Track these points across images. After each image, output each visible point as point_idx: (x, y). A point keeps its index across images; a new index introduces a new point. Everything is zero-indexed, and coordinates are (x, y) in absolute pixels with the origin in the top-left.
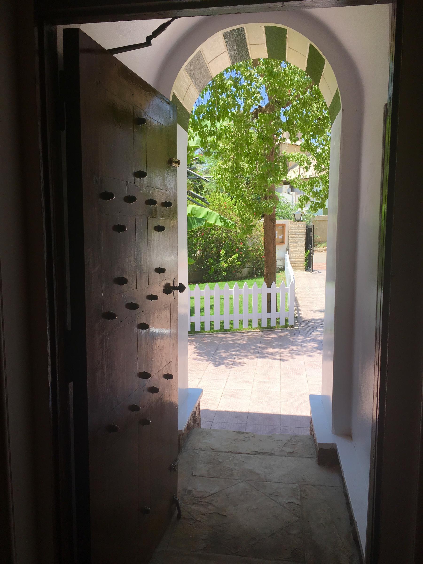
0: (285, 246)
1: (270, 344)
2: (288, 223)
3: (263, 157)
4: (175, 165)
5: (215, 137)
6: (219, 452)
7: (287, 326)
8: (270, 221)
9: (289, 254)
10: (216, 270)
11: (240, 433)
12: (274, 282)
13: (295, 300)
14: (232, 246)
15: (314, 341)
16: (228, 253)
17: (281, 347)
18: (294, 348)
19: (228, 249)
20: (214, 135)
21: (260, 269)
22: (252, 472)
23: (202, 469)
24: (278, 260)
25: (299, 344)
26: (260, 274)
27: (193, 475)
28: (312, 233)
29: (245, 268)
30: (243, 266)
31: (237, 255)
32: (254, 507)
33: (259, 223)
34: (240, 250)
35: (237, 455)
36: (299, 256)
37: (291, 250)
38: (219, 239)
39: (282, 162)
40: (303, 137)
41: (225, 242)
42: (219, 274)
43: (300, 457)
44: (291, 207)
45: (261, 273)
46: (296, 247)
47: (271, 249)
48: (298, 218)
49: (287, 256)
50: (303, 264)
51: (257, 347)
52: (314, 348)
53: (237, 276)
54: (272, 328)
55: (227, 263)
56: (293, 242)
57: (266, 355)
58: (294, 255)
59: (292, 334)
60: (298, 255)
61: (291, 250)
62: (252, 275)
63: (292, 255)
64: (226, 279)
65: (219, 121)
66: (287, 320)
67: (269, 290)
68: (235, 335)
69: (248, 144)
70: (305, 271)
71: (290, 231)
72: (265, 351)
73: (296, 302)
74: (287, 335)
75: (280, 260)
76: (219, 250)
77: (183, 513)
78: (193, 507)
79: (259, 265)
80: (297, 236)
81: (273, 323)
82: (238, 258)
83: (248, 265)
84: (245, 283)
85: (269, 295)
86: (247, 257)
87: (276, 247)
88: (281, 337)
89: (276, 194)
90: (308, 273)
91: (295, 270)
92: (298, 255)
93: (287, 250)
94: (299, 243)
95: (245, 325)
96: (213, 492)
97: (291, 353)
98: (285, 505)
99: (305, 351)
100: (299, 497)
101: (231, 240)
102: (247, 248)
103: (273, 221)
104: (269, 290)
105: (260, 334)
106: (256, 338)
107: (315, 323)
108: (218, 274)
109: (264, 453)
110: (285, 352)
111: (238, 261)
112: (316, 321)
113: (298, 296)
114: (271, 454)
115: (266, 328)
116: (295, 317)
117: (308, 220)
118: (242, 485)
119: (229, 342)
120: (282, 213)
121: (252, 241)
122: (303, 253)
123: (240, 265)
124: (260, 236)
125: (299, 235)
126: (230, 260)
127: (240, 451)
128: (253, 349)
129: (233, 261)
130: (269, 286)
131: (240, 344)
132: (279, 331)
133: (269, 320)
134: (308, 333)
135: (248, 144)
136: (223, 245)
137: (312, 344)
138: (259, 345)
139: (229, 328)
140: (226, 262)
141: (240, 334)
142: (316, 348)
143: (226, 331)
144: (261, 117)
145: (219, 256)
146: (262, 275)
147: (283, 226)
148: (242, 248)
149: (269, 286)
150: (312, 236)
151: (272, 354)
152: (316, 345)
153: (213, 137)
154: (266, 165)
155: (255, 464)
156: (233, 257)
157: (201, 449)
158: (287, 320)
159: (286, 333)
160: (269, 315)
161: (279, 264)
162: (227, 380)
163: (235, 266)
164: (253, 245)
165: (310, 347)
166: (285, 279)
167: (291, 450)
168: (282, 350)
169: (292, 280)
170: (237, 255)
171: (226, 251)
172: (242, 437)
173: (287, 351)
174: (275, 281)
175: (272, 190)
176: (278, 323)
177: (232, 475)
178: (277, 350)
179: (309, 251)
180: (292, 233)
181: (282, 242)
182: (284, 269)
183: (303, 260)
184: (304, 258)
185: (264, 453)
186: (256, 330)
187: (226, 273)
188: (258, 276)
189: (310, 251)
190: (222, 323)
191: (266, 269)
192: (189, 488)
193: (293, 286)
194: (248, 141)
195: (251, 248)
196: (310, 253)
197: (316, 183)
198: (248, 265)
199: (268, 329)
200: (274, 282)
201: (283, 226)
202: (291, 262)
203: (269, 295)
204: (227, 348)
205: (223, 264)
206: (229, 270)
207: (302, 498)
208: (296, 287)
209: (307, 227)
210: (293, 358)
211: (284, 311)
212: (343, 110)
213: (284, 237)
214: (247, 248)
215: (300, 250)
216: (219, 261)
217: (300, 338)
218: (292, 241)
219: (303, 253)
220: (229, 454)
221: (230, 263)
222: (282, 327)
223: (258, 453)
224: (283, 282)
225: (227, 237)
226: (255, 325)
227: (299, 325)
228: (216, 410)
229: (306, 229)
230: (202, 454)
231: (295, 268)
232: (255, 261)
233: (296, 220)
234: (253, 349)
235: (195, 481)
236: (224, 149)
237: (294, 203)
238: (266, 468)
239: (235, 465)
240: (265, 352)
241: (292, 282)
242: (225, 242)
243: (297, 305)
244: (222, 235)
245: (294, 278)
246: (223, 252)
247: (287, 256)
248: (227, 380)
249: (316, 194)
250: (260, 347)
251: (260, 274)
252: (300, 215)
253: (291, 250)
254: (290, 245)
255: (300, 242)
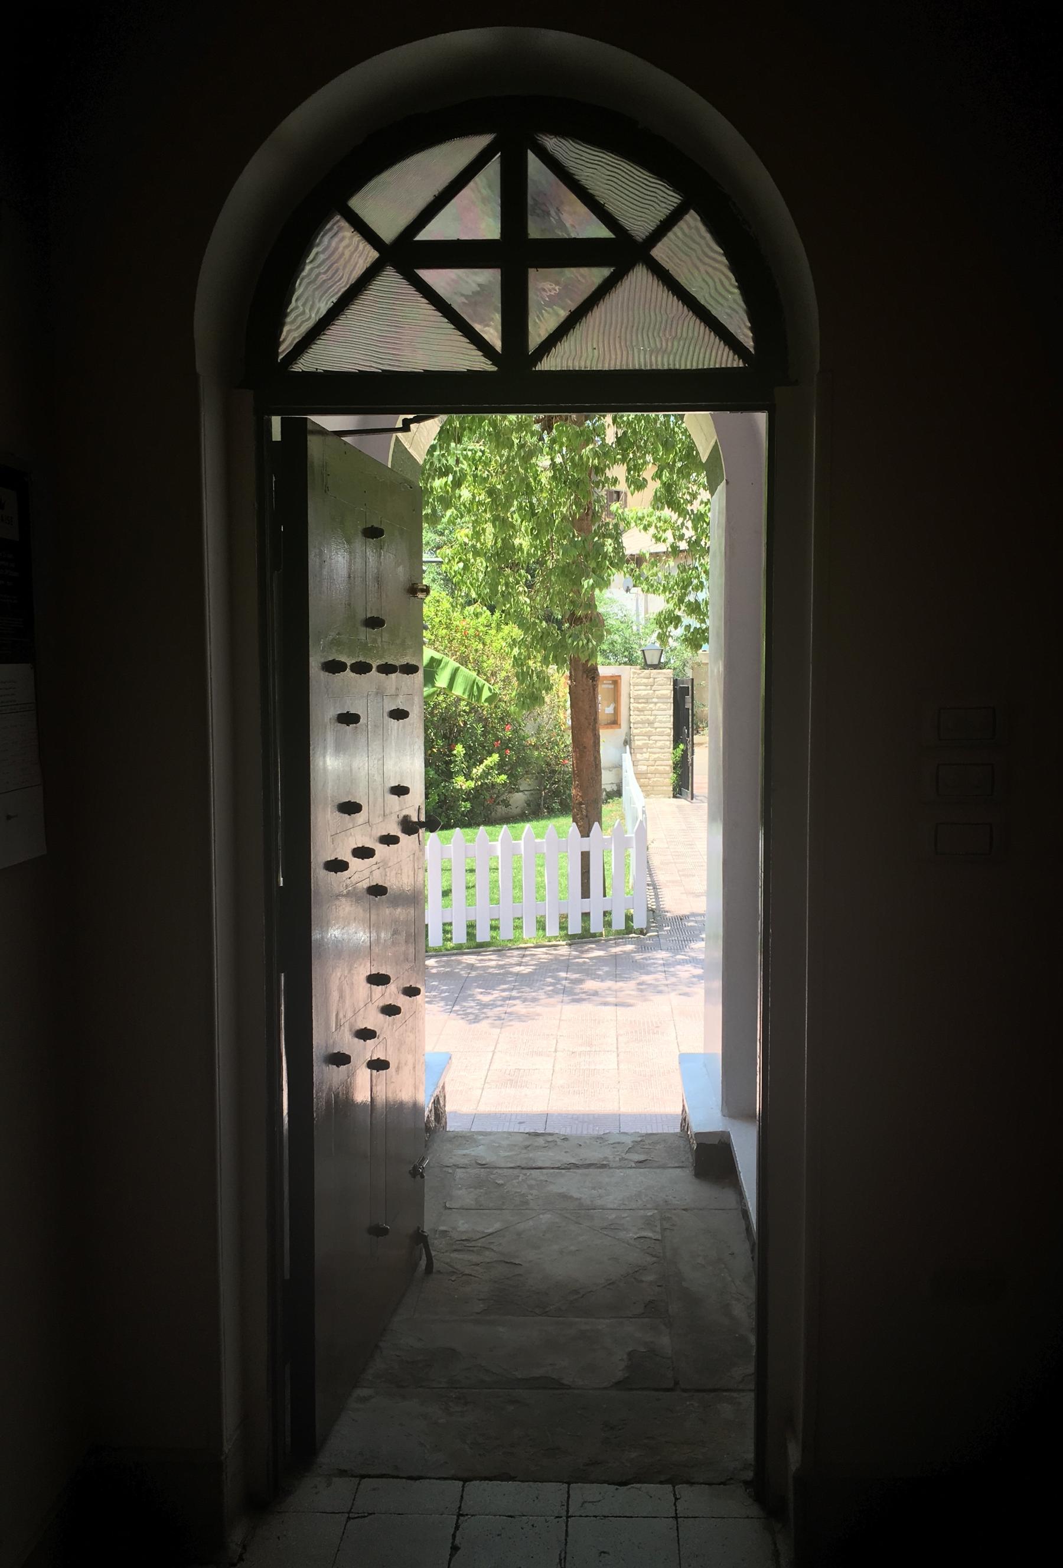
0: (620, 733)
1: (588, 971)
2: (628, 674)
3: (565, 523)
4: (420, 595)
5: (451, 477)
6: (496, 1168)
7: (629, 930)
8: (585, 679)
9: (636, 749)
10: (443, 798)
11: (537, 1135)
12: (596, 824)
13: (649, 868)
14: (484, 734)
15: (694, 961)
16: (475, 752)
17: (616, 977)
18: (647, 978)
19: (474, 742)
20: (446, 474)
21: (556, 793)
22: (565, 1197)
23: (464, 1196)
24: (605, 769)
25: (660, 969)
26: (556, 806)
27: (446, 1208)
28: (688, 698)
29: (518, 791)
30: (512, 787)
31: (496, 757)
32: (573, 1248)
33: (560, 679)
34: (505, 746)
35: (533, 1171)
36: (659, 759)
37: (637, 743)
38: (450, 717)
39: (610, 536)
40: (658, 475)
41: (465, 723)
42: (450, 808)
43: (658, 1167)
44: (635, 628)
45: (561, 804)
46: (649, 736)
47: (589, 741)
48: (652, 659)
49: (627, 758)
50: (669, 779)
51: (559, 980)
52: (694, 976)
53: (499, 814)
54: (594, 935)
55: (472, 779)
56: (642, 722)
57: (584, 996)
58: (646, 756)
59: (643, 948)
60: (656, 756)
61: (637, 743)
62: (536, 810)
63: (639, 756)
64: (470, 821)
65: (459, 441)
66: (629, 918)
67: (585, 844)
68: (504, 955)
69: (529, 492)
70: (674, 797)
71: (633, 693)
72: (578, 988)
73: (651, 875)
74: (633, 952)
75: (610, 769)
76: (449, 745)
77: (436, 1265)
78: (455, 1255)
79: (555, 783)
80: (651, 706)
81: (596, 925)
82: (501, 767)
83: (526, 784)
84: (527, 828)
85: (585, 857)
86: (523, 761)
87: (599, 739)
88: (616, 956)
89: (600, 610)
90: (681, 802)
91: (647, 796)
92: (656, 756)
93: (627, 742)
94: (656, 725)
95: (529, 934)
96: (490, 1231)
97: (641, 990)
98: (632, 1242)
99: (673, 984)
100: (658, 1229)
101: (480, 719)
102: (524, 738)
103: (592, 673)
104: (585, 844)
105: (564, 950)
106: (556, 959)
107: (696, 922)
108: (447, 809)
109: (589, 1166)
110: (628, 987)
111: (499, 774)
112: (699, 919)
113: (655, 861)
114: (603, 1166)
115: (581, 937)
116: (648, 910)
117: (678, 663)
118: (546, 1217)
119: (491, 970)
120: (612, 643)
121: (535, 720)
122: (667, 750)
123: (504, 785)
124: (556, 709)
125: (656, 703)
126: (477, 771)
127: (540, 1164)
128: (551, 984)
129: (486, 774)
130: (585, 832)
131: (517, 974)
132: (608, 939)
133: (586, 916)
134: (680, 946)
135: (529, 492)
136: (459, 731)
137: (688, 967)
138: (563, 974)
139: (488, 940)
140: (468, 777)
141: (516, 953)
142: (698, 977)
143: (481, 945)
144: (561, 432)
145: (451, 762)
146: (565, 809)
147: (615, 681)
148: (510, 740)
149: (585, 832)
150: (688, 706)
151: (596, 993)
152: (699, 971)
153: (444, 480)
154: (573, 544)
155: (570, 1185)
156: (486, 762)
157: (458, 1167)
158: (629, 918)
159: (629, 947)
160: (586, 905)
161: (607, 780)
162: (494, 1052)
163: (493, 785)
164: (539, 731)
165: (687, 975)
166: (623, 817)
167: (642, 1157)
168: (620, 984)
169: (640, 817)
170: (496, 757)
171: (467, 747)
172: (541, 1141)
173: (632, 984)
174: (599, 820)
175: (591, 604)
176: (608, 924)
177: (527, 1203)
178: (609, 984)
179: (682, 746)
180: (637, 699)
181: (614, 722)
182: (618, 793)
183: (668, 768)
184: (671, 762)
185: (589, 1166)
186: (554, 943)
187: (469, 805)
188: (552, 813)
189: (686, 744)
190: (471, 926)
191: (573, 791)
192: (442, 1228)
193: (642, 831)
194: (528, 485)
195: (533, 740)
196: (685, 751)
197: (695, 581)
198: (526, 784)
199: (584, 937)
200: (596, 824)
201: (615, 681)
202: (639, 775)
203: (585, 857)
204: (489, 981)
205: (461, 783)
206: (475, 797)
207: (664, 1230)
208: (650, 836)
209: (675, 682)
210: (645, 1000)
211: (621, 894)
212: (727, 483)
213: (616, 710)
214: (524, 738)
215: (659, 744)
216: (449, 776)
217: (661, 955)
218: (639, 718)
219: (667, 750)
220: (516, 1172)
221: (480, 778)
222: (618, 932)
223: (577, 1166)
224: (619, 824)
225: (470, 712)
226: (552, 929)
227: (660, 927)
228: (474, 1112)
229: (675, 690)
230: (460, 1173)
231: (648, 790)
232: (544, 772)
233: (647, 666)
234: (551, 984)
235: (453, 1218)
236: (472, 503)
237: (642, 616)
238: (594, 1188)
239: (531, 1187)
240: (578, 991)
241: (641, 822)
242: (465, 723)
243: (653, 881)
244: (456, 707)
245: (644, 812)
246: (459, 749)
247: (627, 758)
248: (494, 1052)
249: (695, 609)
250: (566, 979)
251: (556, 806)
252: (658, 654)
253: (638, 742)
254: (634, 731)
255: (660, 722)
